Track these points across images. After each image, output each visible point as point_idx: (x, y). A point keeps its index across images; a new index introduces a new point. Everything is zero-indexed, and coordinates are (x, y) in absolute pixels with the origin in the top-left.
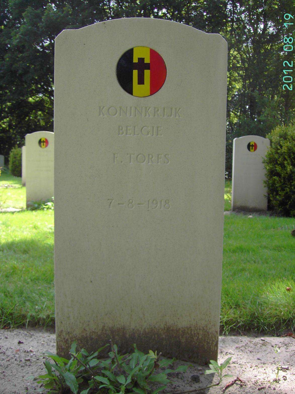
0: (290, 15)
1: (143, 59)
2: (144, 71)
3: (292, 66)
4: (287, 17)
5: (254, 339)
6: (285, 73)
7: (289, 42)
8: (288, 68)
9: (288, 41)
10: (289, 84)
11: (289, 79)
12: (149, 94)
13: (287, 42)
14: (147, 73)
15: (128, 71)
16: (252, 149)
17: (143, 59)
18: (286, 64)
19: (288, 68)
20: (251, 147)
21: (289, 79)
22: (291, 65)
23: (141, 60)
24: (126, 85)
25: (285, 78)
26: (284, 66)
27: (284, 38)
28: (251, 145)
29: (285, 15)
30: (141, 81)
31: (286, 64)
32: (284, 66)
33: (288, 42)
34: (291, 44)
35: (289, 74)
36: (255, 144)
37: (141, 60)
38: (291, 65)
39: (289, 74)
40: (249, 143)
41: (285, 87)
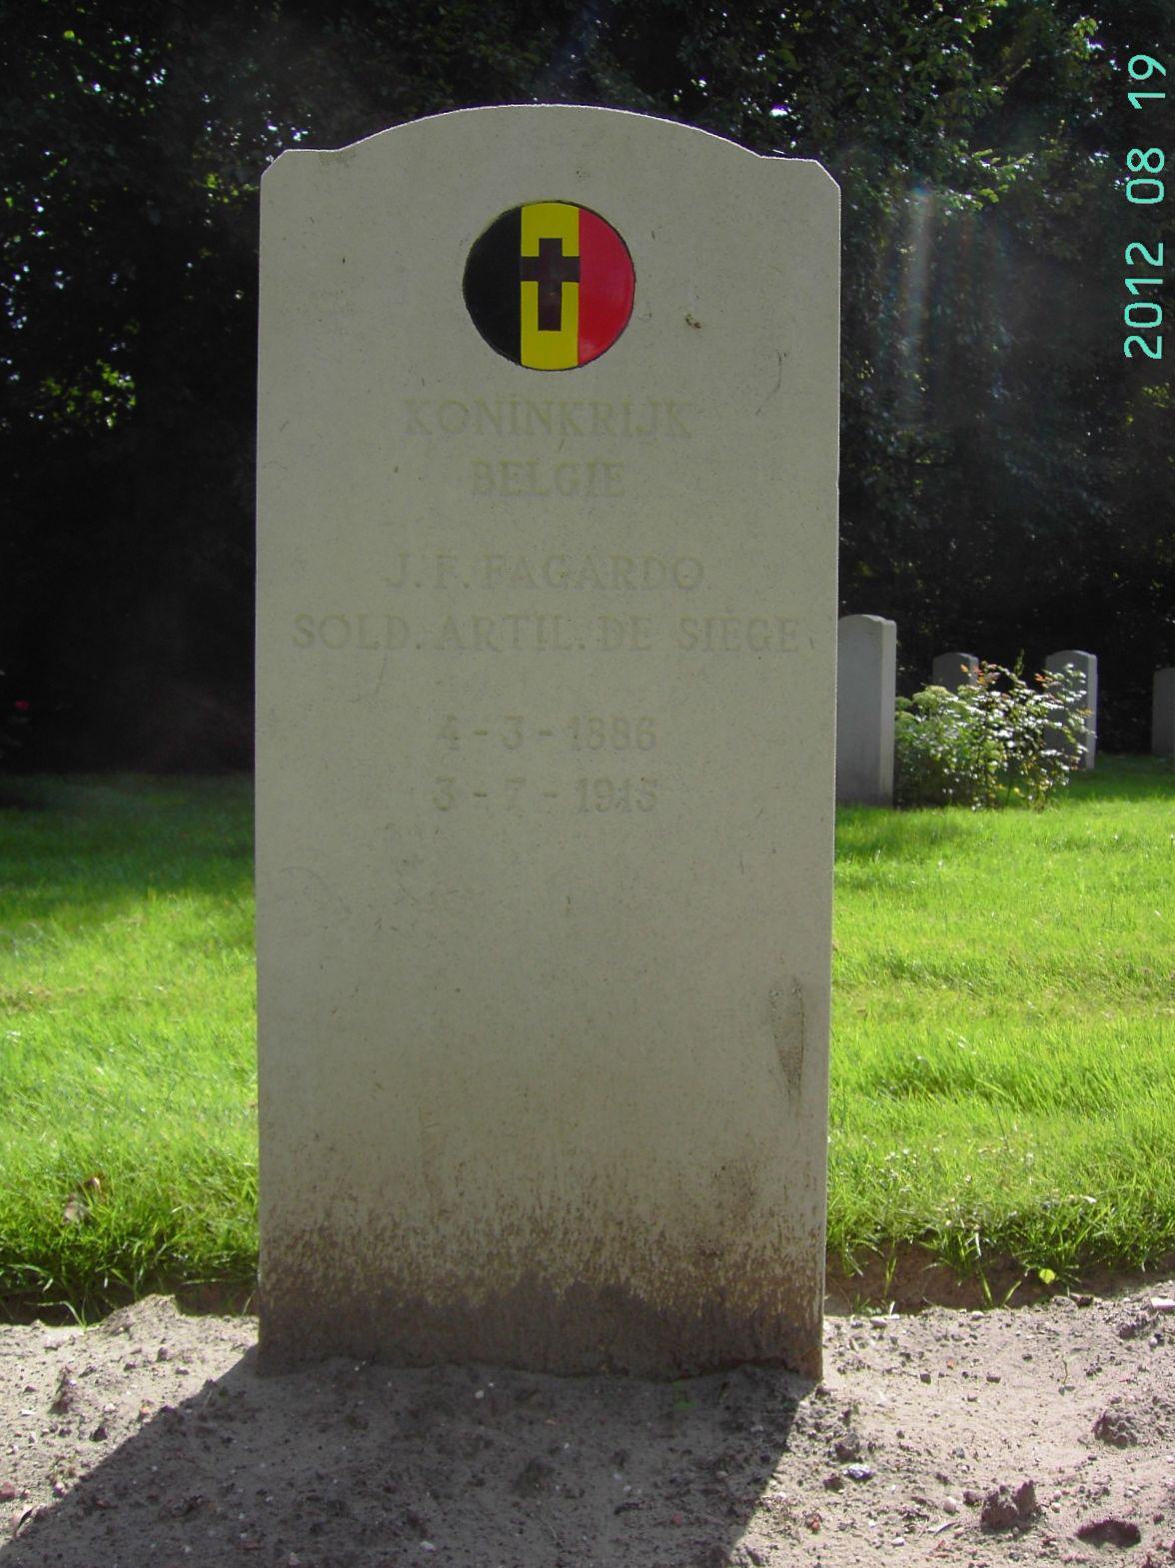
0: (1151, 62)
1: (557, 243)
2: (1148, 683)
3: (1160, 262)
4: (1141, 67)
5: (1072, 812)
6: (1134, 291)
7: (1149, 169)
8: (1140, 269)
9: (1144, 163)
10: (1149, 337)
11: (1150, 315)
12: (576, 364)
13: (1139, 168)
14: (570, 292)
15: (499, 282)
16: (550, 319)
17: (557, 243)
18: (1135, 253)
19: (1140, 269)
20: (529, 292)
21: (1150, 315)
22: (1155, 257)
23: (550, 246)
24: (503, 335)
25: (1131, 312)
26: (1129, 261)
27: (1126, 183)
28: (529, 248)
29: (1134, 60)
30: (550, 319)
31: (1135, 253)
32: (1129, 261)
33: (1144, 152)
34: (1137, 332)
35: (1145, 293)
36: (592, 224)
37: (550, 246)
38: (1155, 257)
39: (1145, 293)
40: (508, 226)
41: (1134, 346)
